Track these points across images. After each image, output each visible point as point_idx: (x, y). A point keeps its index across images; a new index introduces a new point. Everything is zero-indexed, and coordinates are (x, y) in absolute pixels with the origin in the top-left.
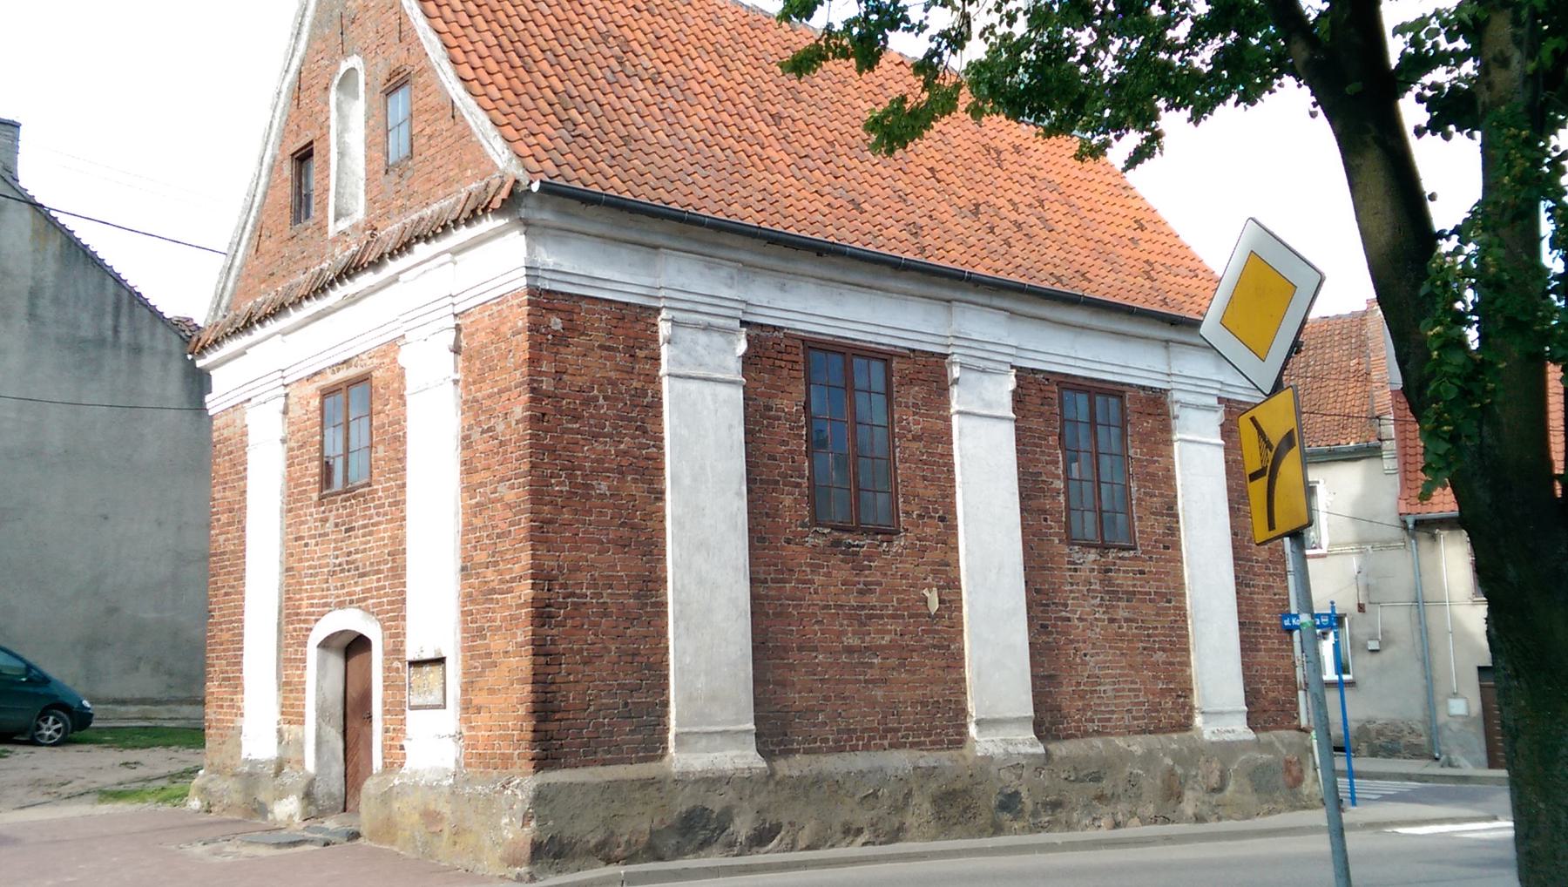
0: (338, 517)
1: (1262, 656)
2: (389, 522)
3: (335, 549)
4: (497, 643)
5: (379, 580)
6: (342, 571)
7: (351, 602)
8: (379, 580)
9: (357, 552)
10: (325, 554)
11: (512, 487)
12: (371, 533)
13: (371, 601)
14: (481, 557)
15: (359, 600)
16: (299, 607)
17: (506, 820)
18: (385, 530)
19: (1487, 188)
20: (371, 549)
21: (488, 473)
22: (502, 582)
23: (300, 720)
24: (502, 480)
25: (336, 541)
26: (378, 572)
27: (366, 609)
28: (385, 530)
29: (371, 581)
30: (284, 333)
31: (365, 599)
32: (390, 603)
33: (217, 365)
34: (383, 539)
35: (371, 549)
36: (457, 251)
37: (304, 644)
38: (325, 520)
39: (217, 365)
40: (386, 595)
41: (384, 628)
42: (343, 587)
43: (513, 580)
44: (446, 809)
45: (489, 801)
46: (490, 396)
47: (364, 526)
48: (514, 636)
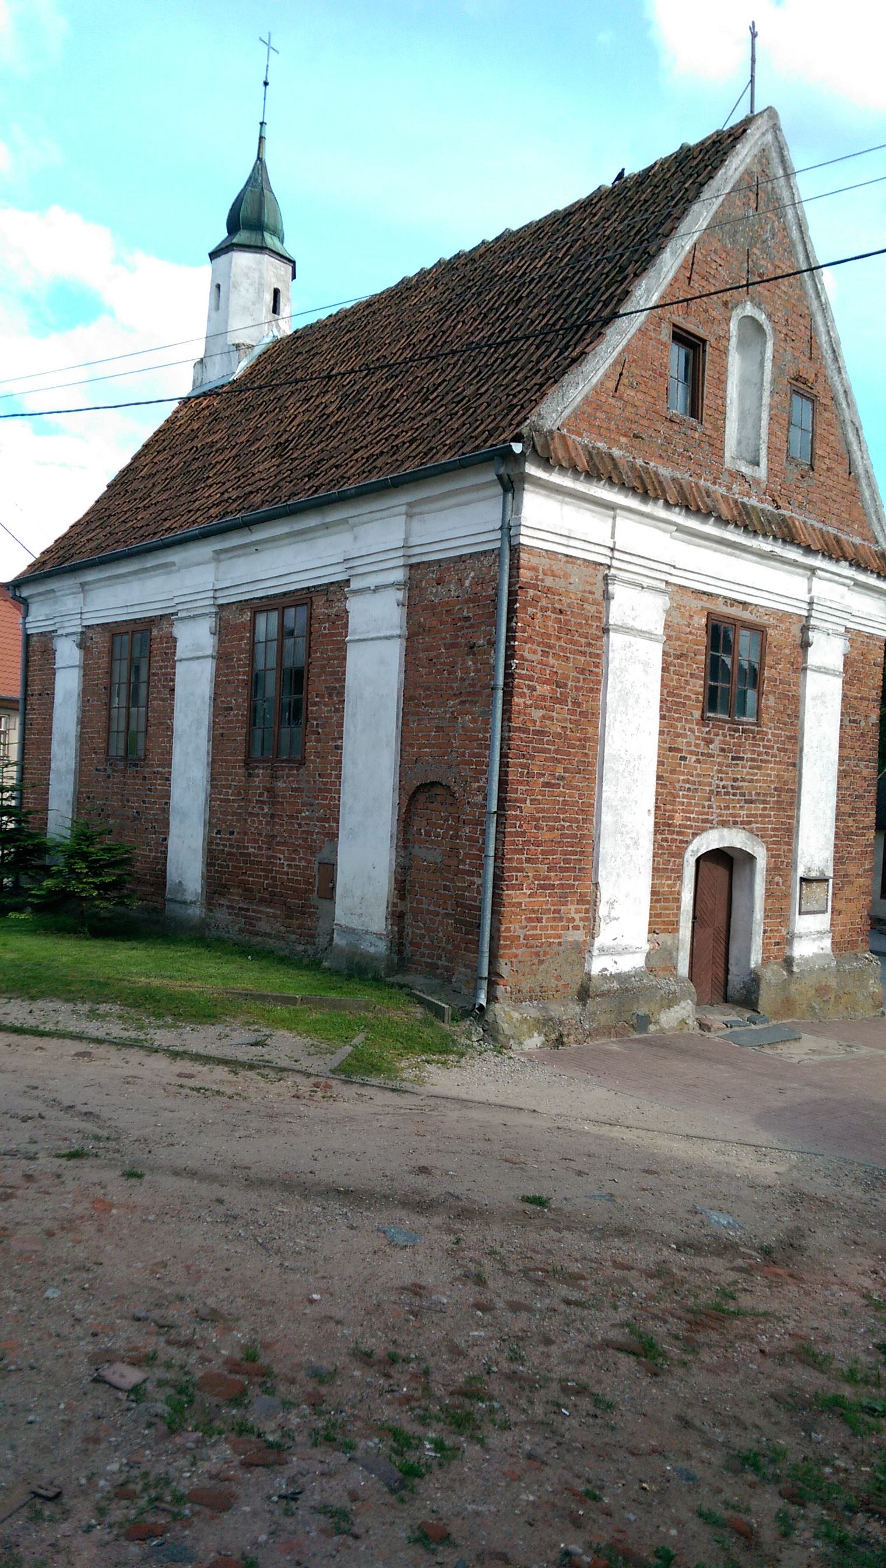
0: (724, 742)
1: (772, 770)
2: (776, 762)
3: (719, 771)
4: (852, 869)
5: (765, 809)
6: (727, 793)
7: (735, 823)
8: (765, 809)
9: (743, 780)
10: (711, 774)
11: (867, 767)
12: (759, 768)
13: (754, 825)
14: (846, 809)
15: (742, 823)
16: (671, 818)
17: (872, 981)
18: (772, 769)
19: (518, 231)
20: (758, 781)
21: (853, 752)
22: (858, 828)
23: (673, 927)
24: (861, 760)
25: (720, 764)
26: (765, 802)
27: (751, 831)
28: (772, 769)
29: (757, 809)
30: (680, 529)
31: (750, 823)
32: (773, 829)
33: (538, 483)
34: (769, 775)
35: (758, 781)
36: (857, 584)
37: (681, 856)
38: (708, 742)
39: (538, 483)
40: (769, 822)
41: (768, 849)
42: (727, 808)
43: (863, 828)
44: (833, 983)
45: (862, 970)
46: (856, 698)
47: (752, 760)
48: (862, 865)
